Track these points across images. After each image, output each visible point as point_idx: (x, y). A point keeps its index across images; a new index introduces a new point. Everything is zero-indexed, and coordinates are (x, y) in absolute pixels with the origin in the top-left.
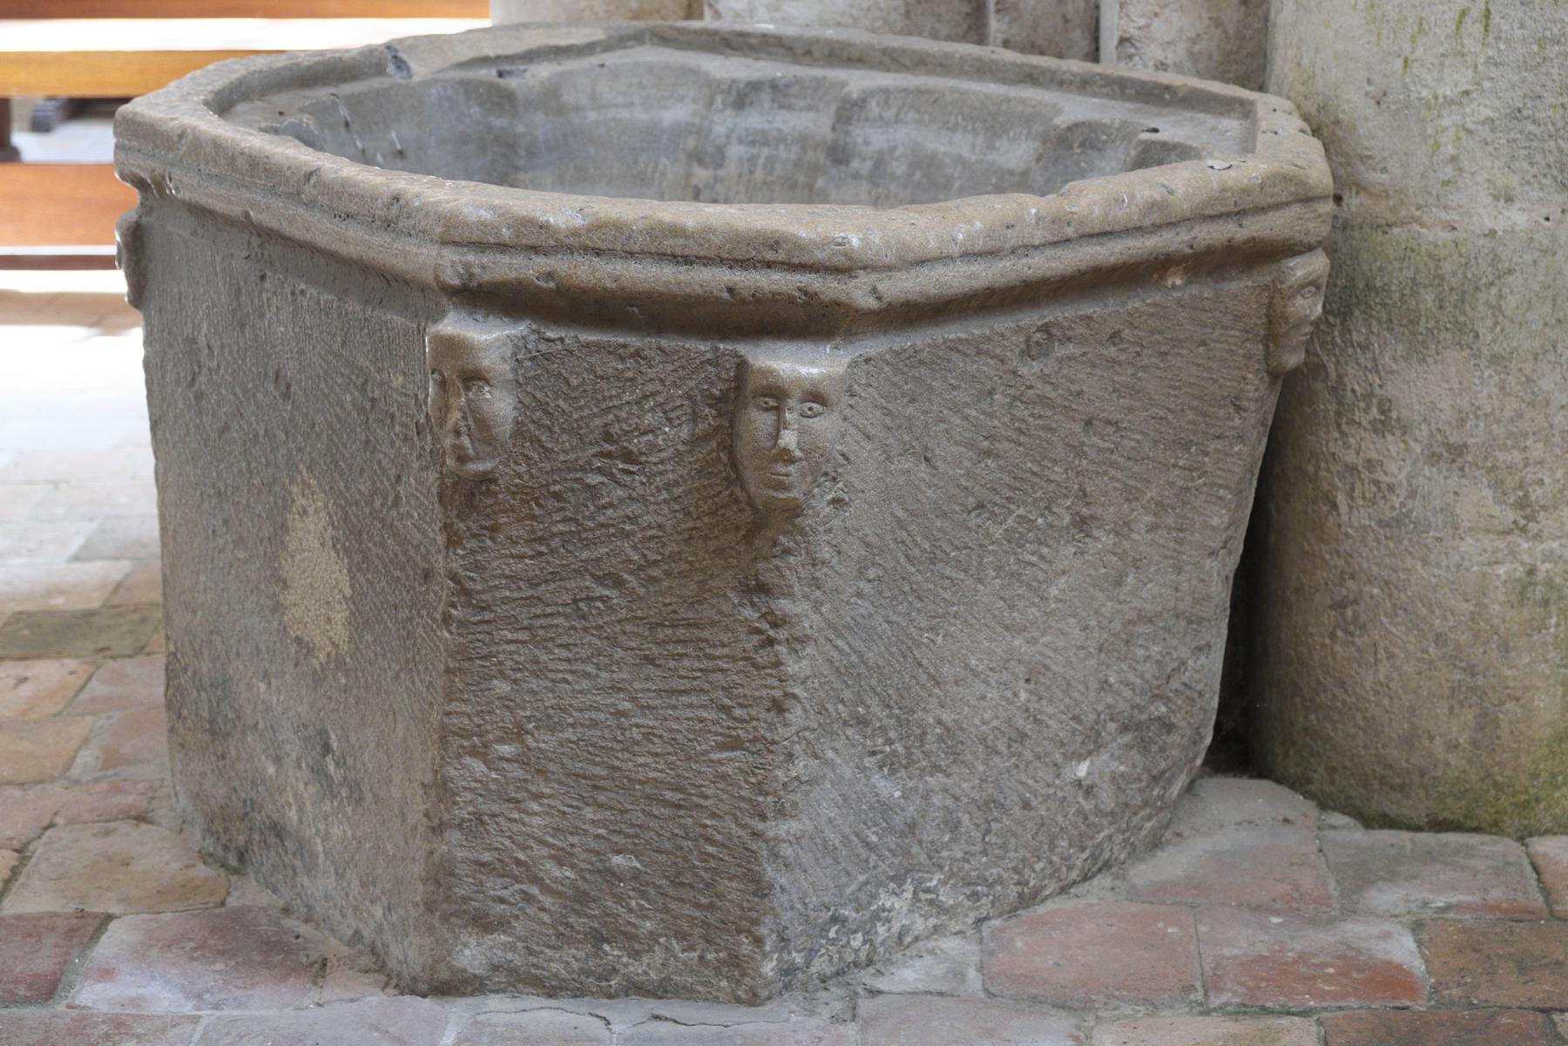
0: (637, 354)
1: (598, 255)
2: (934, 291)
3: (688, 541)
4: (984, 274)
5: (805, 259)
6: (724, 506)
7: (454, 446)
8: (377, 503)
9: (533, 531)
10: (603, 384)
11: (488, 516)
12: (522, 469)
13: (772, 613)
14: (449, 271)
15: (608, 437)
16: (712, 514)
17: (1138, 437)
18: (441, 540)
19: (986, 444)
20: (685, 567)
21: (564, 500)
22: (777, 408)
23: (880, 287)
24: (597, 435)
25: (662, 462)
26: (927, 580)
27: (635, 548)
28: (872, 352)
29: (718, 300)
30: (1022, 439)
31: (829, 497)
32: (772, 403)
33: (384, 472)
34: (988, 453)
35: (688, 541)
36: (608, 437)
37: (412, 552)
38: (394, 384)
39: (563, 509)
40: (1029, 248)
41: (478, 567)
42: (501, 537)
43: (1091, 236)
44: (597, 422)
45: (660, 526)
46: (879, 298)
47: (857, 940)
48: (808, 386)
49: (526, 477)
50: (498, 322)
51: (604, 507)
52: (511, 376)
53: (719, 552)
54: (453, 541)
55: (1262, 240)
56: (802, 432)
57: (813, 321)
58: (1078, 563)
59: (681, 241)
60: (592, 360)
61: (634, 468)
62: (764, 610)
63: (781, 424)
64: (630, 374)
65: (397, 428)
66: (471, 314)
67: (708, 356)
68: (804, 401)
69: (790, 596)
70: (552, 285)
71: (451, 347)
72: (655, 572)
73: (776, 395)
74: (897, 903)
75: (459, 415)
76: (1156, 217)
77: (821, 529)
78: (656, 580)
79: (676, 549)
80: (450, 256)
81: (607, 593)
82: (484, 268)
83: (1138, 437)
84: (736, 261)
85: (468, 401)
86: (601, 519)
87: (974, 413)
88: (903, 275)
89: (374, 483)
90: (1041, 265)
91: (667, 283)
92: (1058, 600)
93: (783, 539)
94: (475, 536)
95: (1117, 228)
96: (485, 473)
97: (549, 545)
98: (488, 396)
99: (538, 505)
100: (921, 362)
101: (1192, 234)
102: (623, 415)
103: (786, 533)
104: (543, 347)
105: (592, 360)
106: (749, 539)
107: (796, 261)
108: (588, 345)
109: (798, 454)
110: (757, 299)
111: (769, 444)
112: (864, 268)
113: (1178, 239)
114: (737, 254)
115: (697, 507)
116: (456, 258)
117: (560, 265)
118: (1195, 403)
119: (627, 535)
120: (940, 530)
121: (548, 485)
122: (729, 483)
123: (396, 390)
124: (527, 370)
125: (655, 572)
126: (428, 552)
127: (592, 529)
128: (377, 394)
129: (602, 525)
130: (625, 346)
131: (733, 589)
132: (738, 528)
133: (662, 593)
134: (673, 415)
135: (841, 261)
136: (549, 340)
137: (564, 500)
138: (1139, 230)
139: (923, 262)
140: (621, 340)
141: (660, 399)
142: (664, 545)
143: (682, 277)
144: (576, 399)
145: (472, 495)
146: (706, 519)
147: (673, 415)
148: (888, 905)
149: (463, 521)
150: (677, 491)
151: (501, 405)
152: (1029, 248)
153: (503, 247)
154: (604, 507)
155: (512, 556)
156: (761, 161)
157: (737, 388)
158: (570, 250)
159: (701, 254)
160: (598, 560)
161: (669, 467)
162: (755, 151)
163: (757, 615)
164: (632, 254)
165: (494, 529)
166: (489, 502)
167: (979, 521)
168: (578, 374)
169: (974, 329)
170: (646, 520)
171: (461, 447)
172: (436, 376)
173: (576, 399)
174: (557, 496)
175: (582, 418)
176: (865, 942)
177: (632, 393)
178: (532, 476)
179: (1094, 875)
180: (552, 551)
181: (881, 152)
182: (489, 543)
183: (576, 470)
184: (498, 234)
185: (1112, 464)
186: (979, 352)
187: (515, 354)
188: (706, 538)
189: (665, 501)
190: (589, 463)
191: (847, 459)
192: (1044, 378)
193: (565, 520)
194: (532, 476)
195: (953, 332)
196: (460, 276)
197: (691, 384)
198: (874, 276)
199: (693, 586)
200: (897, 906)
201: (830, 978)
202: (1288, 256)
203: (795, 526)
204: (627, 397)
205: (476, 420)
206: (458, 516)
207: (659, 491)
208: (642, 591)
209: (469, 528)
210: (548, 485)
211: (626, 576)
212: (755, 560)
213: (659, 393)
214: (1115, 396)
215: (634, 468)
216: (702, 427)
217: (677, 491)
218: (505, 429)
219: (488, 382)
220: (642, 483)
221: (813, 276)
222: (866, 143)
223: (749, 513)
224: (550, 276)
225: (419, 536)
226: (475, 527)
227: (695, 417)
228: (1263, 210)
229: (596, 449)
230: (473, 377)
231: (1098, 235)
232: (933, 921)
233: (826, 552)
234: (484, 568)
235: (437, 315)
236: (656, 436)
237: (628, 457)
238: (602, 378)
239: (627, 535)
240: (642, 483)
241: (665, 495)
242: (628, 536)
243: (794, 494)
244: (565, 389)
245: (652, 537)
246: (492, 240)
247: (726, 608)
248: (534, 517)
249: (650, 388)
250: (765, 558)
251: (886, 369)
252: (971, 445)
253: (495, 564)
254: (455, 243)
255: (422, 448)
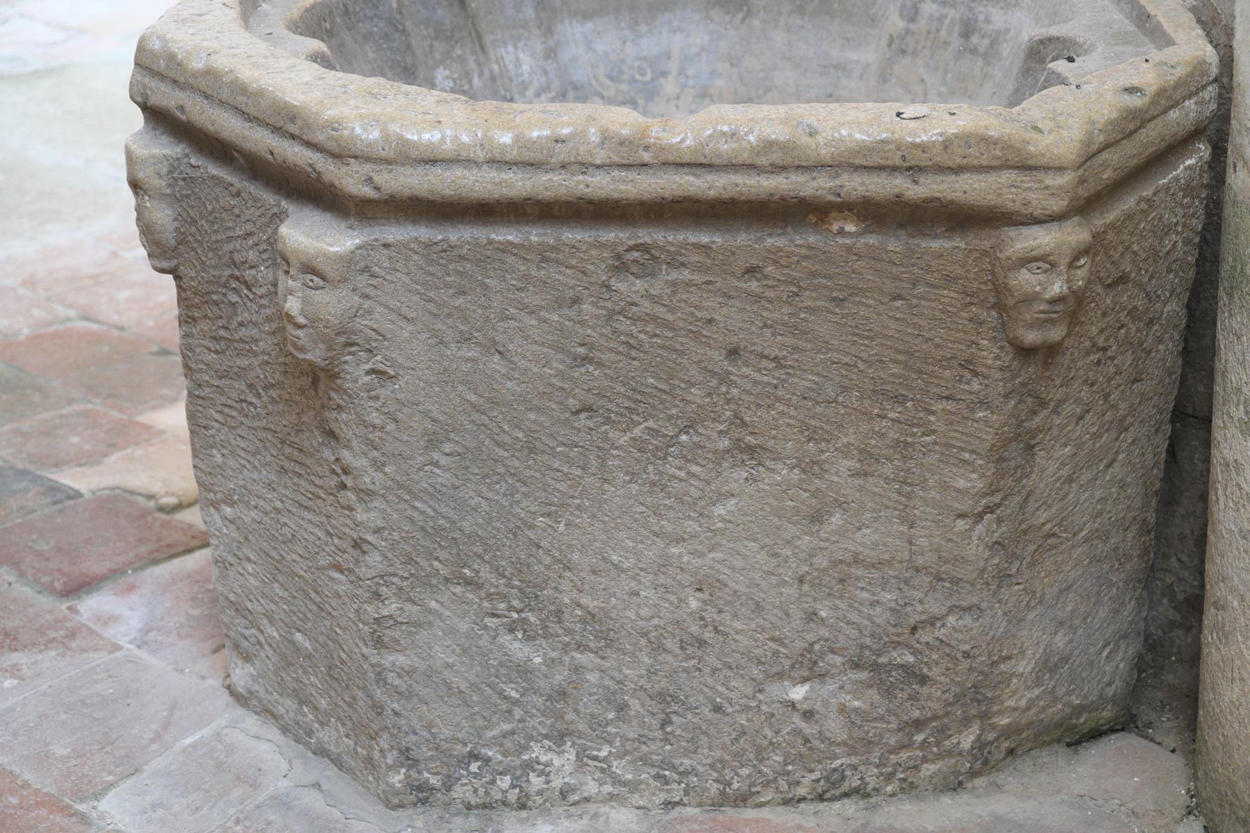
2: (447, 192)
4: (518, 184)
17: (816, 379)
19: (582, 350)
23: (376, 178)
26: (529, 467)
28: (390, 239)
30: (633, 353)
31: (367, 367)
34: (586, 359)
40: (585, 167)
43: (682, 165)
46: (377, 189)
47: (505, 782)
55: (952, 202)
56: (305, 301)
58: (750, 489)
59: (244, 99)
74: (563, 762)
76: (777, 157)
83: (816, 379)
87: (556, 318)
88: (409, 171)
90: (601, 185)
92: (723, 520)
95: (717, 161)
98: (148, 205)
100: (462, 258)
101: (838, 182)
112: (356, 157)
113: (815, 184)
118: (901, 357)
120: (534, 422)
138: (750, 167)
148: (543, 759)
152: (585, 167)
156: (947, 21)
162: (944, 11)
167: (590, 424)
169: (536, 235)
176: (513, 787)
179: (834, 799)
181: (998, 33)
185: (778, 399)
186: (545, 259)
187: (170, 172)
192: (648, 296)
195: (508, 235)
198: (368, 167)
200: (557, 762)
201: (477, 807)
202: (1010, 225)
214: (768, 333)
222: (987, 21)
228: (958, 170)
231: (689, 165)
232: (608, 788)
251: (416, 257)
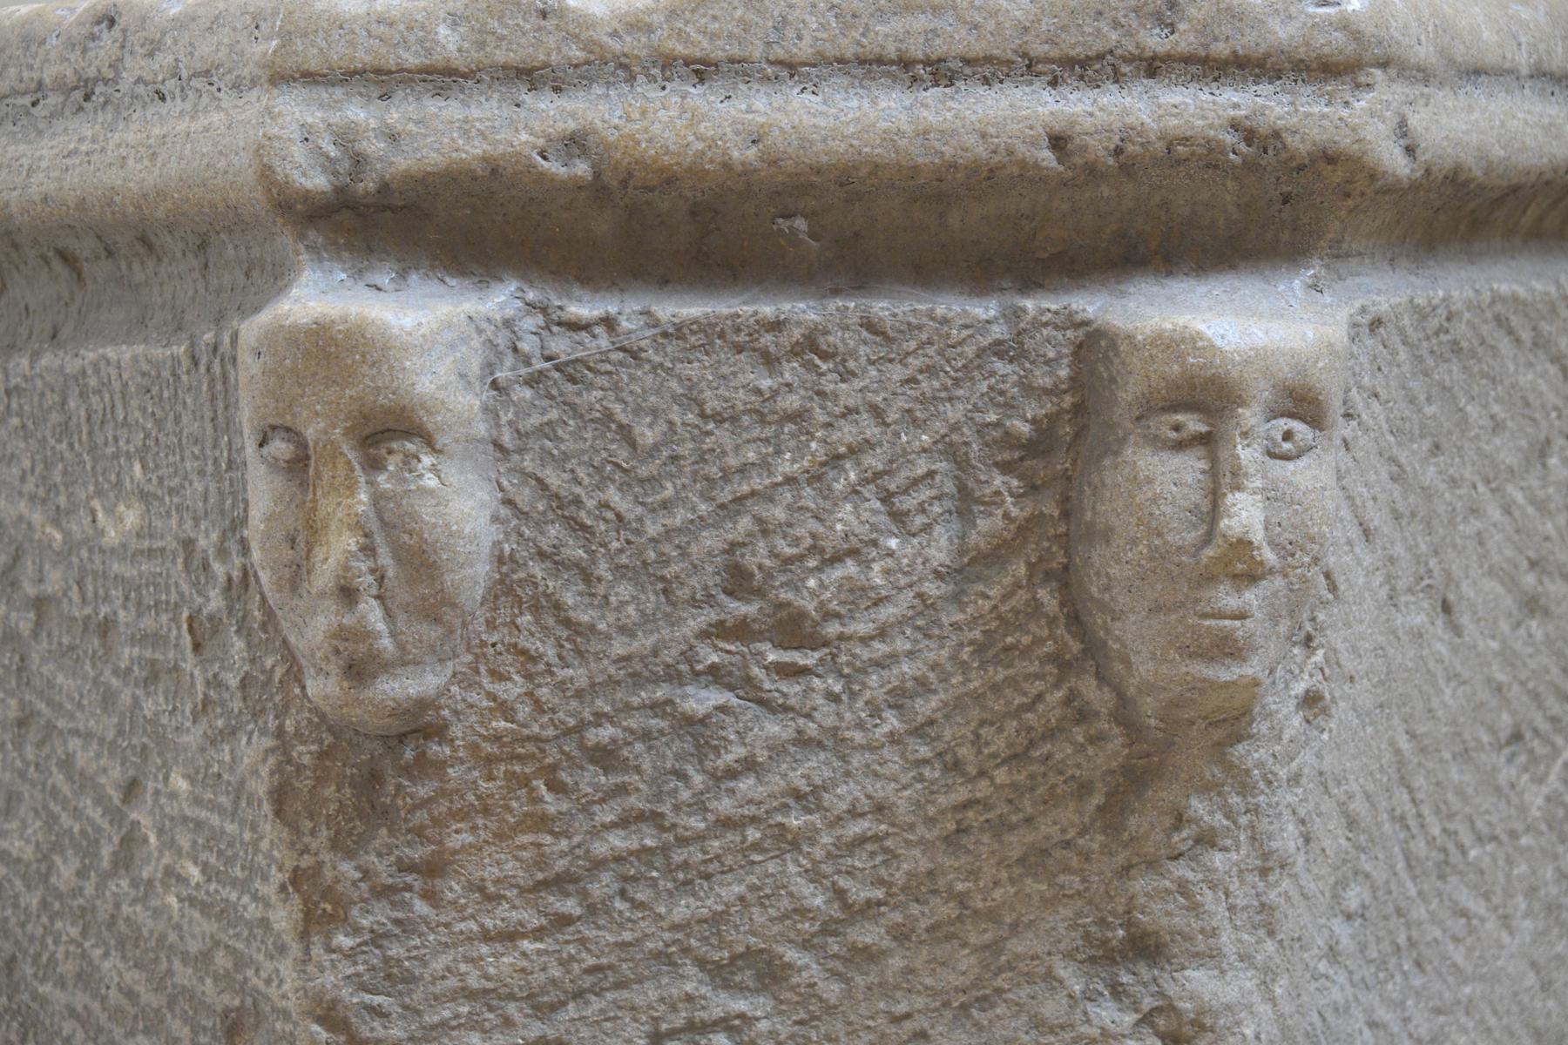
0: (810, 345)
1: (701, 77)
3: (951, 841)
5: (1246, 41)
6: (1050, 734)
7: (341, 634)
8: (65, 871)
9: (541, 862)
10: (722, 436)
11: (419, 832)
12: (513, 689)
13: (1169, 1008)
14: (298, 153)
15: (738, 581)
16: (1016, 758)
18: (284, 918)
20: (948, 910)
21: (624, 766)
22: (1205, 440)
23: (1414, 121)
24: (710, 577)
25: (882, 633)
27: (814, 875)
29: (1028, 174)
32: (1194, 424)
33: (84, 782)
35: (951, 841)
36: (738, 581)
37: (184, 975)
38: (112, 536)
39: (622, 790)
41: (395, 978)
42: (453, 888)
44: (711, 540)
45: (880, 809)
46: (1410, 150)
48: (1286, 373)
49: (524, 711)
50: (434, 286)
51: (731, 774)
52: (481, 429)
53: (1035, 861)
54: (321, 910)
56: (1272, 496)
57: (1263, 212)
60: (692, 370)
61: (808, 659)
62: (1148, 1003)
63: (1220, 482)
64: (792, 402)
65: (127, 653)
66: (358, 274)
67: (999, 331)
68: (1273, 414)
69: (1211, 957)
70: (582, 168)
71: (328, 350)
72: (869, 934)
73: (1201, 402)
75: (351, 542)
77: (1283, 773)
78: (869, 955)
79: (924, 865)
80: (296, 112)
81: (741, 1005)
82: (393, 137)
84: (1069, 63)
85: (378, 499)
86: (725, 806)
89: (51, 821)
91: (888, 137)
93: (1198, 807)
94: (384, 892)
96: (423, 704)
97: (584, 894)
98: (431, 481)
99: (556, 787)
102: (779, 513)
103: (1209, 788)
104: (561, 345)
105: (692, 370)
106: (1112, 816)
107: (1221, 49)
108: (679, 331)
109: (1269, 556)
110: (1129, 160)
111: (1192, 537)
114: (1074, 43)
115: (977, 741)
116: (314, 117)
117: (601, 111)
119: (788, 842)
121: (581, 727)
122: (1064, 666)
123: (120, 552)
124: (522, 413)
125: (869, 934)
126: (241, 962)
127: (700, 837)
128: (55, 579)
129: (727, 823)
130: (776, 326)
131: (1069, 955)
132: (1084, 789)
133: (885, 989)
134: (907, 503)
135: (1335, 43)
136: (575, 326)
137: (624, 766)
139: (1478, 72)
140: (767, 310)
141: (874, 461)
142: (892, 856)
143: (930, 117)
144: (653, 481)
145: (375, 777)
146: (1001, 776)
147: (907, 503)
149: (350, 855)
150: (925, 707)
151: (460, 504)
153: (442, 78)
154: (731, 774)
155: (486, 936)
157: (1078, 409)
158: (625, 69)
159: (978, 48)
160: (717, 919)
161: (902, 645)
163: (1130, 1018)
164: (791, 67)
165: (433, 869)
166: (423, 791)
168: (655, 412)
170: (845, 794)
171: (363, 634)
172: (280, 447)
173: (653, 481)
174: (605, 757)
175: (668, 533)
177: (800, 450)
178: (539, 707)
180: (592, 910)
182: (421, 907)
183: (656, 680)
184: (427, 43)
187: (489, 367)
188: (1000, 828)
189: (894, 739)
190: (689, 656)
191: (1333, 588)
193: (623, 822)
194: (539, 707)
196: (329, 165)
197: (954, 413)
199: (967, 961)
203: (1229, 767)
204: (786, 465)
205: (398, 552)
206: (335, 844)
207: (876, 712)
208: (832, 990)
209: (366, 874)
210: (581, 727)
211: (791, 955)
212: (1126, 871)
213: (869, 445)
215: (808, 659)
216: (986, 525)
217: (925, 707)
218: (472, 576)
219: (429, 442)
220: (833, 698)
221: (1265, 88)
223: (1117, 743)
224: (575, 143)
225: (209, 926)
226: (383, 870)
227: (966, 503)
229: (709, 616)
230: (389, 430)
233: (1287, 839)
234: (410, 979)
235: (278, 277)
236: (866, 564)
237: (793, 629)
238: (718, 419)
239: (788, 842)
240: (833, 698)
241: (892, 721)
242: (795, 846)
243: (1252, 668)
244: (622, 455)
245: (861, 840)
246: (411, 59)
247: (1052, 1008)
248: (542, 822)
249: (846, 433)
250: (1152, 864)
252: (1511, 583)
253: (439, 964)
254: (309, 78)
255: (215, 682)
